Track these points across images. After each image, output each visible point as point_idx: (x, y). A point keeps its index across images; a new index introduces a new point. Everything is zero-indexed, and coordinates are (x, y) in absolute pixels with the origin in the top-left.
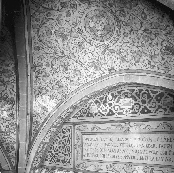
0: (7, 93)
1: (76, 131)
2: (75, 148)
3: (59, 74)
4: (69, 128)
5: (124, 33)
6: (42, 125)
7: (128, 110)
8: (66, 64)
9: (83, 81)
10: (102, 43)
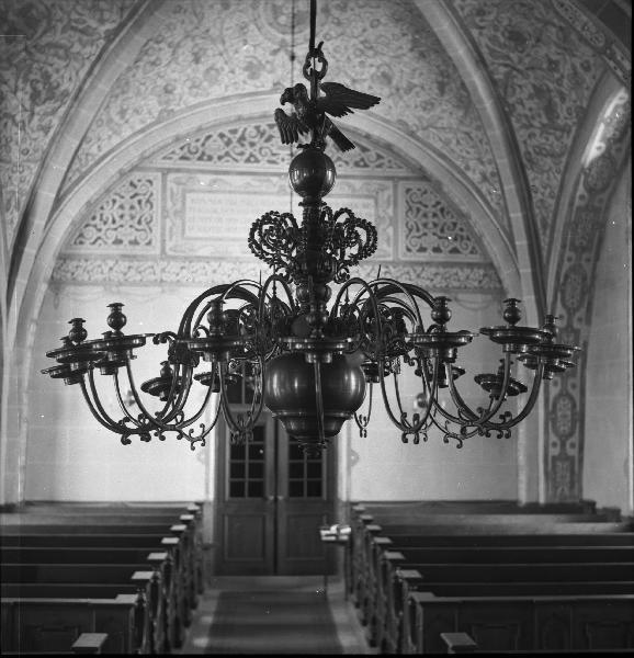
0: (63, 77)
1: (170, 185)
2: (164, 217)
3: (179, 67)
4: (151, 178)
5: (327, 34)
6: (97, 163)
7: (279, 161)
8: (201, 53)
9: (217, 91)
10: (281, 36)
